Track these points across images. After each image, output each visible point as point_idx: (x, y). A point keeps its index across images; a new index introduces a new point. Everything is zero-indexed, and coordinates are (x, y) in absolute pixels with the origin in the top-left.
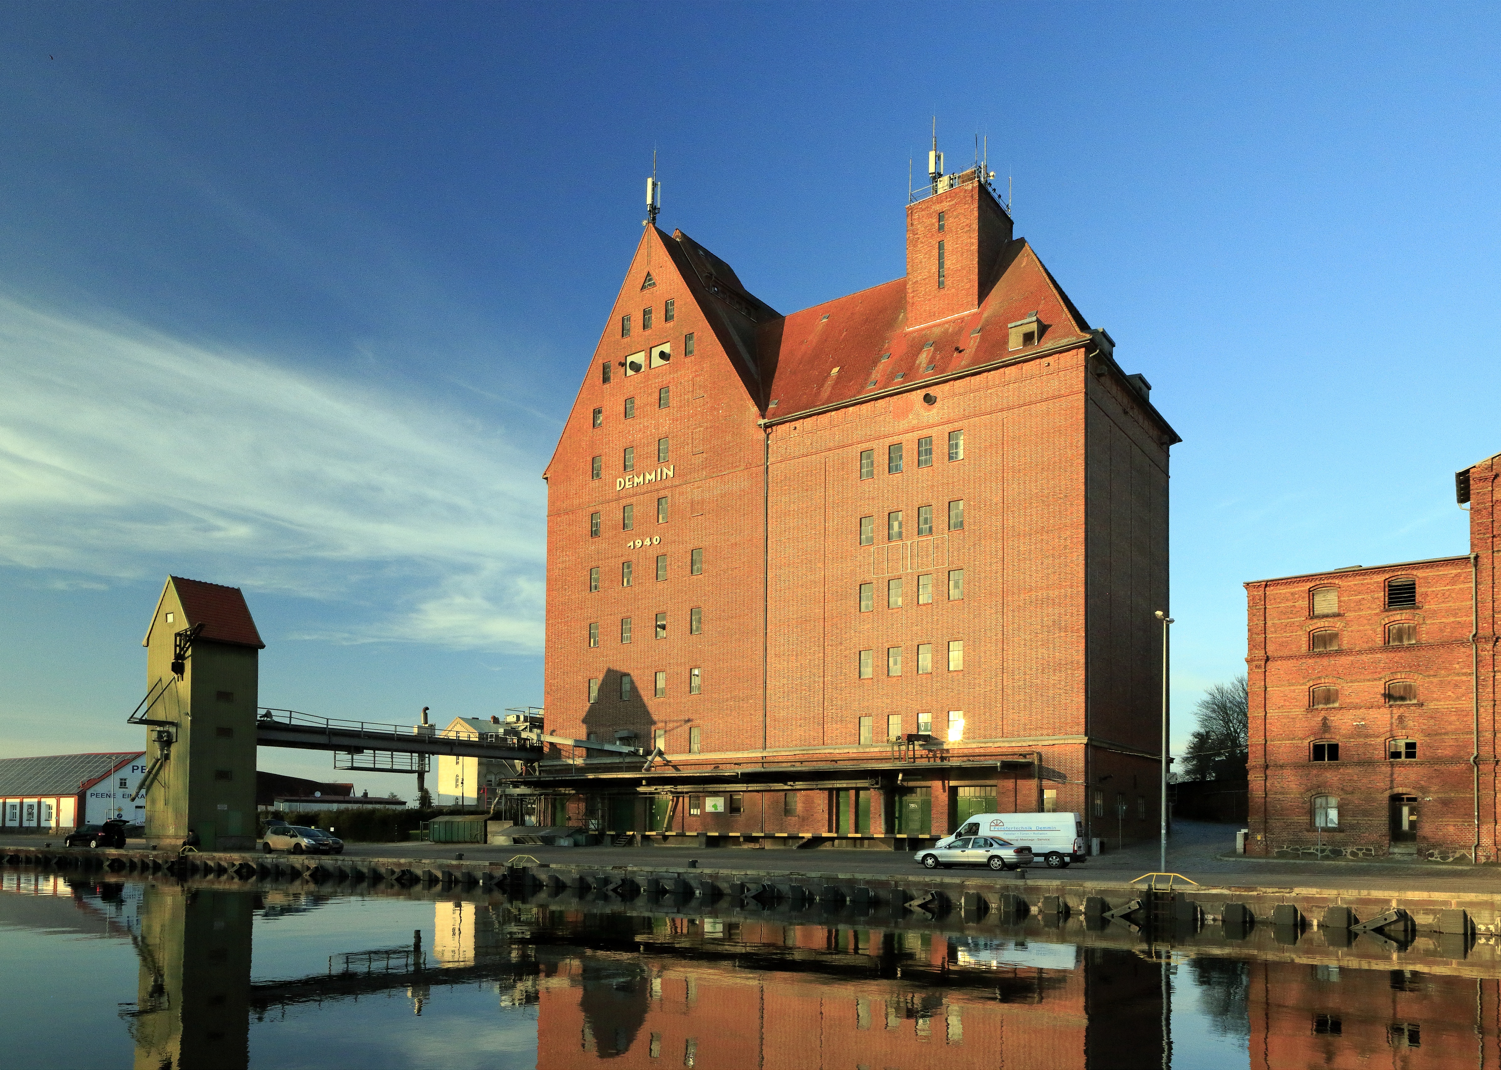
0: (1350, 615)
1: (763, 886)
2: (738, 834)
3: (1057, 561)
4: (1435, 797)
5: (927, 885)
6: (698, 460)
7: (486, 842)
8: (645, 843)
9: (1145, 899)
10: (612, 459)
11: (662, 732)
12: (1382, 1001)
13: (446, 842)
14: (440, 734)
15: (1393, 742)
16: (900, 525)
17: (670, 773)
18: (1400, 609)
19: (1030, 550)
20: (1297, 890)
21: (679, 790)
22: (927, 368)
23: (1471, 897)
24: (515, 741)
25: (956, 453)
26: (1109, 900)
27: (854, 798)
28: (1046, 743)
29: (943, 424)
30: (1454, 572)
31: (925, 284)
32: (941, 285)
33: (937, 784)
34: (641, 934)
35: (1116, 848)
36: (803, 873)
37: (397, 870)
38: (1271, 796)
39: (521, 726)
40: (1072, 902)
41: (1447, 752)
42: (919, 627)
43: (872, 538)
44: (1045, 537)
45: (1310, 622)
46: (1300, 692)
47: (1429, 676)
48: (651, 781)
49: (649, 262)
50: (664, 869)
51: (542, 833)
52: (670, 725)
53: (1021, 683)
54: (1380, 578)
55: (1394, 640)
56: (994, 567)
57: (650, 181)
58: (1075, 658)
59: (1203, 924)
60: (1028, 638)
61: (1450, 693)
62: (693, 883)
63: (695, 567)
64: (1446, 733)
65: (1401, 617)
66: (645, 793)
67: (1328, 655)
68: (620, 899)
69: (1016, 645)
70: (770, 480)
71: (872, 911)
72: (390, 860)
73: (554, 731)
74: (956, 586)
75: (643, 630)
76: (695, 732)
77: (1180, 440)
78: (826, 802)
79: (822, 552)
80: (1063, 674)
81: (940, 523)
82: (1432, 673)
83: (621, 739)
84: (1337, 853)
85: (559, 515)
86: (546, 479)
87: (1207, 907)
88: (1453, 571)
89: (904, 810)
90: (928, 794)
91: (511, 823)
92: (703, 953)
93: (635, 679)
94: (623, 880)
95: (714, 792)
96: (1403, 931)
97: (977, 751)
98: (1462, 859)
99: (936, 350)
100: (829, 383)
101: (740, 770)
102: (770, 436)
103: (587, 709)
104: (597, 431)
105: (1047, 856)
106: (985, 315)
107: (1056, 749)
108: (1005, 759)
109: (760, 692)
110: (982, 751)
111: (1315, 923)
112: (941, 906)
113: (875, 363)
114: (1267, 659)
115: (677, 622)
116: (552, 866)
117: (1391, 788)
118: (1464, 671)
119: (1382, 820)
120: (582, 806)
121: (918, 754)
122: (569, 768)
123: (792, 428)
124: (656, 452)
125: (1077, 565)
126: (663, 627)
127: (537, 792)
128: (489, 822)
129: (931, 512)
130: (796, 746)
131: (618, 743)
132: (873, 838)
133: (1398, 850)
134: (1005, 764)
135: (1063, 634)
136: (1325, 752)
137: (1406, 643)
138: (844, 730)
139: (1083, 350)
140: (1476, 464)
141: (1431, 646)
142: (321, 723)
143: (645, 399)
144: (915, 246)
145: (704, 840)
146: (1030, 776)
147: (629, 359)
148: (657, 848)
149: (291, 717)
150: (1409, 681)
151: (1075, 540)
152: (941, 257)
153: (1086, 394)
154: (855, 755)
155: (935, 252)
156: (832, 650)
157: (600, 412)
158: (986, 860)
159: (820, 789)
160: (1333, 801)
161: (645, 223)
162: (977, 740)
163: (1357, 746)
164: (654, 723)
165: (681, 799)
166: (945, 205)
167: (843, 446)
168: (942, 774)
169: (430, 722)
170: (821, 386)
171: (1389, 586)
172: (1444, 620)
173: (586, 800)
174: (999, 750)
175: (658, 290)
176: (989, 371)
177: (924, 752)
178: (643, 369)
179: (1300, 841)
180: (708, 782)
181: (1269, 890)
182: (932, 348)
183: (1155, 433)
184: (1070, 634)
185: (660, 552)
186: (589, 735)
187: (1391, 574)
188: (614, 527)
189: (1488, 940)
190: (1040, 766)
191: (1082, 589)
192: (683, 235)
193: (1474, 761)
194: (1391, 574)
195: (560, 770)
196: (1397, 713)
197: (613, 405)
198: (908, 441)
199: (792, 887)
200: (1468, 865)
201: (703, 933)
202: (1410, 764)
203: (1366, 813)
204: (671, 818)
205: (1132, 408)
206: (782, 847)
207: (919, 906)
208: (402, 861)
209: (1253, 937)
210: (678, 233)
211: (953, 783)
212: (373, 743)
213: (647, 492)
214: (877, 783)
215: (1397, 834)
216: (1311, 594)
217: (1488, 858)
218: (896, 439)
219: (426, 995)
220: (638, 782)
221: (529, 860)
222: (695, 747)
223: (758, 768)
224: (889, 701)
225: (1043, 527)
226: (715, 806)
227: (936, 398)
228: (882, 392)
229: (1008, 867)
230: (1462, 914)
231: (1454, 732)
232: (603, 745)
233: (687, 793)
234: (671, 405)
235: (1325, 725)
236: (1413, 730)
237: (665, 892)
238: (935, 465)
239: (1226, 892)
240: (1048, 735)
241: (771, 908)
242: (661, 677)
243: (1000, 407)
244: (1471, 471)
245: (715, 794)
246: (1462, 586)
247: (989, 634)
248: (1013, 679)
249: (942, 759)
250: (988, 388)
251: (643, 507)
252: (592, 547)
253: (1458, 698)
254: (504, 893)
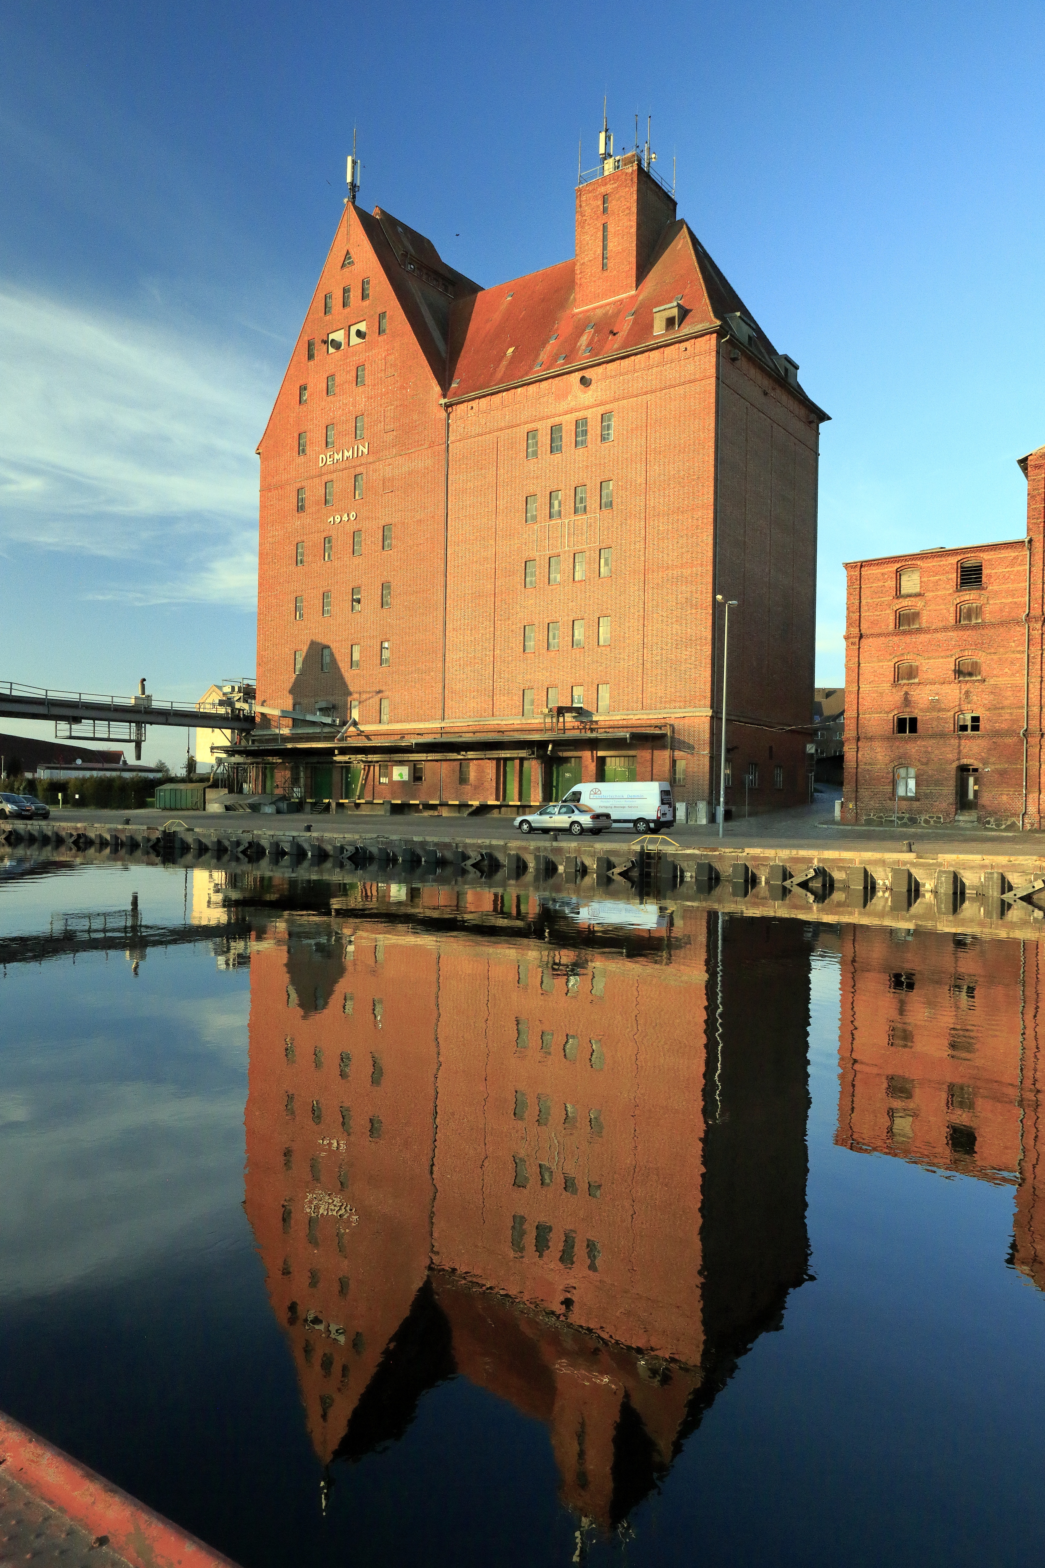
0: (929, 595)
1: (357, 848)
2: (417, 802)
3: (690, 540)
4: (993, 767)
5: (480, 847)
6: (389, 437)
7: (204, 810)
8: (340, 810)
9: (638, 859)
10: (316, 435)
11: (357, 703)
12: (946, 959)
13: (171, 809)
14: (155, 704)
15: (961, 716)
16: (560, 503)
17: (362, 742)
18: (969, 590)
19: (668, 530)
20: (747, 850)
21: (369, 760)
22: (585, 351)
23: (868, 855)
24: (229, 711)
25: (608, 434)
26: (612, 859)
27: (518, 767)
28: (678, 715)
29: (598, 405)
30: (1013, 554)
31: (592, 266)
32: (604, 267)
33: (587, 754)
34: (336, 897)
35: (741, 816)
36: (386, 836)
37: (75, 834)
38: (862, 766)
39: (237, 696)
40: (587, 862)
41: (1003, 726)
42: (574, 603)
43: (536, 516)
44: (680, 517)
45: (896, 601)
46: (887, 668)
47: (990, 653)
48: (343, 751)
49: (348, 240)
50: (281, 833)
51: (250, 801)
52: (364, 696)
53: (659, 658)
54: (953, 560)
55: (964, 619)
56: (637, 546)
57: (349, 159)
58: (704, 634)
59: (682, 881)
60: (665, 615)
61: (1007, 670)
62: (306, 846)
63: (386, 543)
64: (1002, 708)
65: (970, 596)
66: (341, 762)
67: (910, 632)
68: (246, 859)
69: (655, 621)
70: (450, 458)
71: (439, 871)
72: (69, 824)
73: (264, 701)
74: (606, 564)
75: (340, 604)
76: (385, 703)
77: (829, 418)
78: (494, 771)
79: (494, 530)
80: (694, 650)
81: (593, 502)
82: (993, 651)
83: (321, 710)
84: (913, 821)
85: (270, 490)
86: (259, 454)
87: (684, 865)
88: (1011, 554)
89: (560, 779)
90: (580, 763)
91: (226, 791)
92: (392, 917)
93: (334, 650)
94: (250, 843)
95: (400, 761)
96: (824, 886)
97: (621, 722)
98: (1011, 827)
99: (595, 332)
100: (504, 363)
101: (421, 740)
102: (451, 415)
103: (292, 680)
104: (304, 408)
105: (636, 822)
106: (641, 298)
107: (686, 721)
108: (634, 730)
109: (440, 665)
110: (625, 722)
111: (763, 879)
112: (490, 866)
113: (544, 343)
114: (861, 637)
115: (371, 596)
116: (197, 830)
117: (959, 759)
118: (1018, 649)
119: (949, 790)
120: (288, 774)
121: (568, 725)
122: (275, 738)
123: (469, 408)
124: (354, 429)
125: (707, 545)
126: (359, 601)
127: (249, 761)
128: (207, 790)
129: (586, 493)
130: (470, 717)
131: (318, 713)
132: (530, 806)
133: (964, 818)
134: (634, 736)
135: (694, 611)
136: (906, 725)
137: (974, 621)
138: (510, 702)
139: (715, 335)
140: (1033, 451)
141: (993, 625)
142: (39, 694)
143: (344, 377)
144: (583, 227)
145: (389, 807)
146: (664, 747)
147: (331, 337)
148: (351, 815)
149: (11, 689)
150: (975, 659)
151: (705, 520)
152: (604, 238)
153: (717, 378)
154: (519, 726)
155: (600, 234)
156: (501, 625)
157: (305, 389)
158: (568, 825)
159: (489, 759)
160: (912, 772)
161: (346, 200)
162: (621, 712)
163: (932, 719)
164: (350, 694)
165: (372, 768)
166: (609, 188)
167: (512, 427)
168: (593, 744)
169: (147, 693)
170: (497, 367)
171: (962, 568)
172: (1003, 600)
173: (292, 769)
174: (639, 722)
175: (356, 268)
176: (636, 354)
177: (577, 724)
178: (342, 348)
179: (885, 810)
180: (394, 751)
181: (727, 850)
182: (593, 330)
183: (802, 412)
184: (699, 610)
185: (356, 528)
186: (294, 705)
187: (962, 556)
188: (317, 503)
189: (884, 892)
190: (672, 738)
191: (710, 568)
192: (383, 212)
193: (1024, 735)
194: (962, 556)
195: (269, 739)
196: (965, 688)
197: (316, 384)
198: (567, 422)
199: (380, 849)
200: (1015, 831)
201: (390, 897)
202: (973, 737)
203: (938, 783)
204: (364, 786)
205: (774, 389)
206: (457, 815)
207: (620, 874)
208: (79, 825)
209: (717, 891)
210: (377, 210)
211: (601, 753)
212: (93, 713)
213: (346, 469)
214: (533, 753)
215: (963, 803)
216: (898, 574)
217: (1032, 825)
218: (557, 420)
219: (143, 957)
220: (330, 752)
221: (180, 825)
222: (385, 718)
223: (439, 739)
224: (548, 674)
225: (679, 508)
226: (401, 775)
227: (591, 380)
228: (544, 374)
229: (584, 831)
230: (863, 871)
231: (1010, 707)
232: (305, 715)
233: (377, 762)
234: (366, 383)
235: (907, 701)
236: (978, 705)
237: (284, 853)
238: (590, 446)
239: (697, 852)
240: (680, 708)
241: (363, 867)
242: (356, 648)
243: (644, 390)
244: (1030, 458)
245: (401, 763)
246: (1019, 568)
247: (632, 610)
248: (652, 654)
249: (592, 730)
250: (635, 371)
251: (341, 484)
252: (297, 522)
253: (1013, 675)
254: (158, 856)
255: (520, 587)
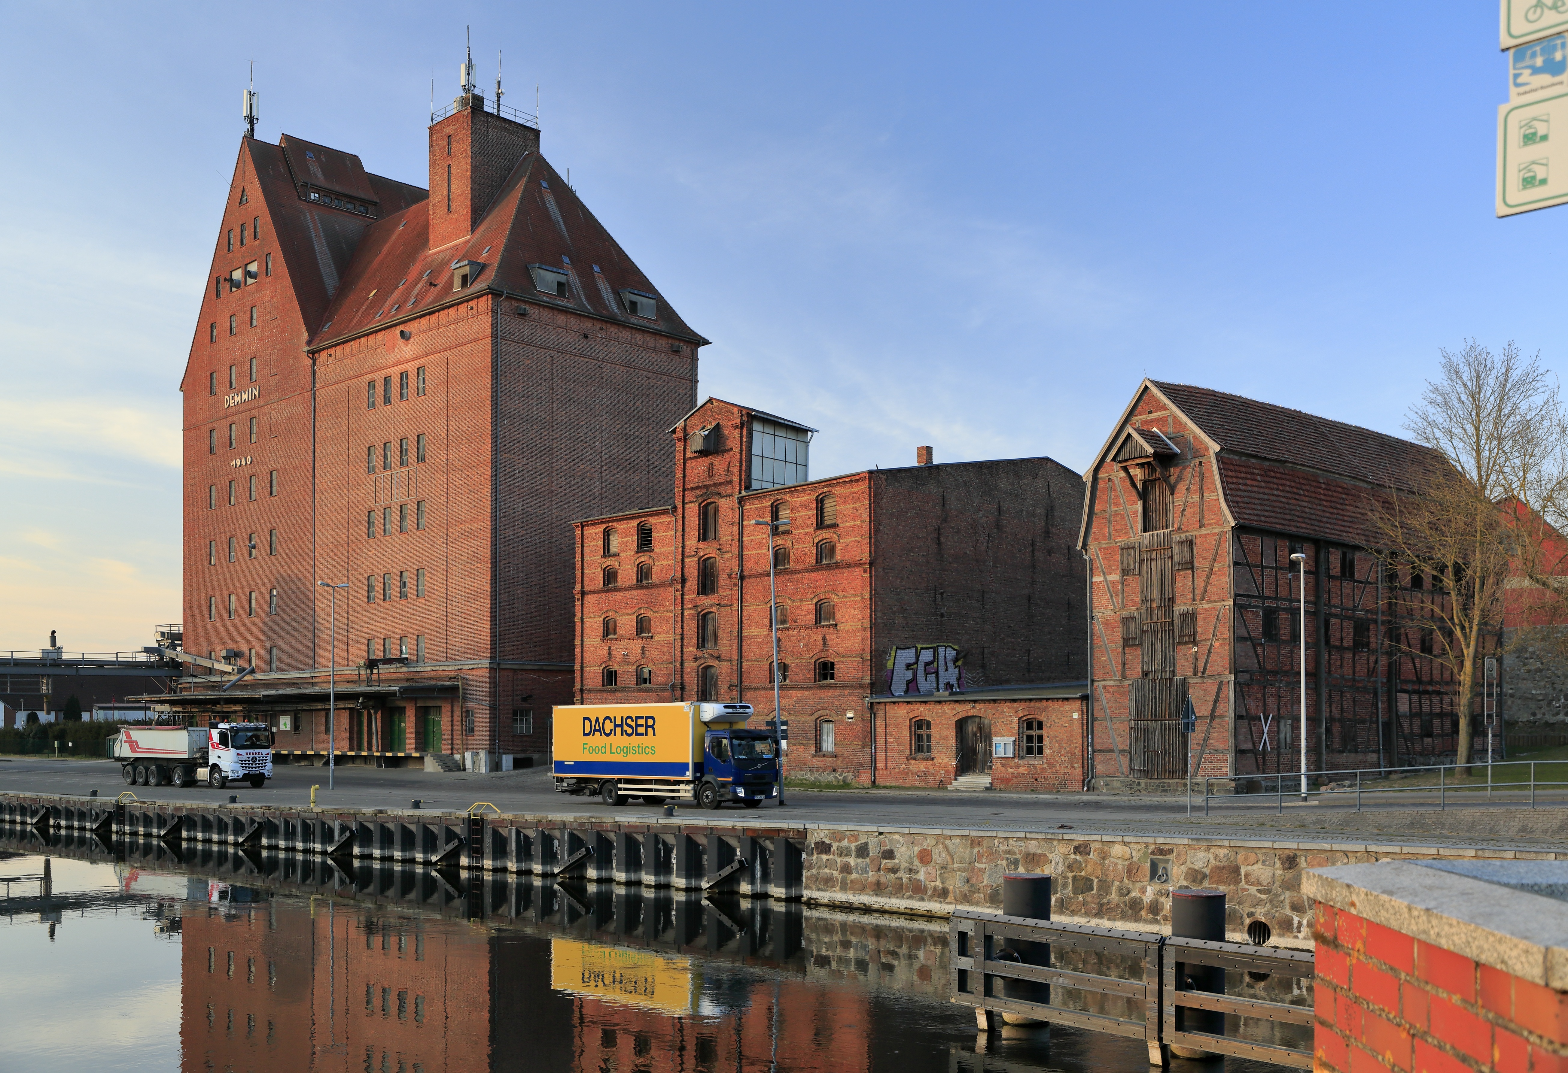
81: (412, 456)
255: (365, 537)
